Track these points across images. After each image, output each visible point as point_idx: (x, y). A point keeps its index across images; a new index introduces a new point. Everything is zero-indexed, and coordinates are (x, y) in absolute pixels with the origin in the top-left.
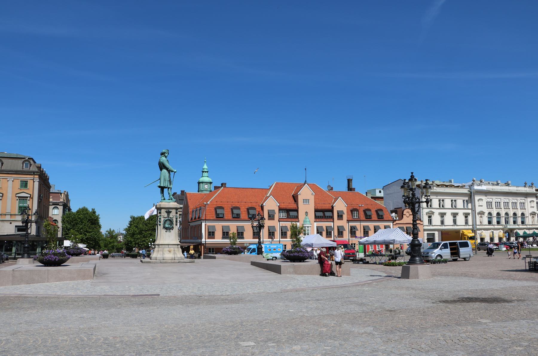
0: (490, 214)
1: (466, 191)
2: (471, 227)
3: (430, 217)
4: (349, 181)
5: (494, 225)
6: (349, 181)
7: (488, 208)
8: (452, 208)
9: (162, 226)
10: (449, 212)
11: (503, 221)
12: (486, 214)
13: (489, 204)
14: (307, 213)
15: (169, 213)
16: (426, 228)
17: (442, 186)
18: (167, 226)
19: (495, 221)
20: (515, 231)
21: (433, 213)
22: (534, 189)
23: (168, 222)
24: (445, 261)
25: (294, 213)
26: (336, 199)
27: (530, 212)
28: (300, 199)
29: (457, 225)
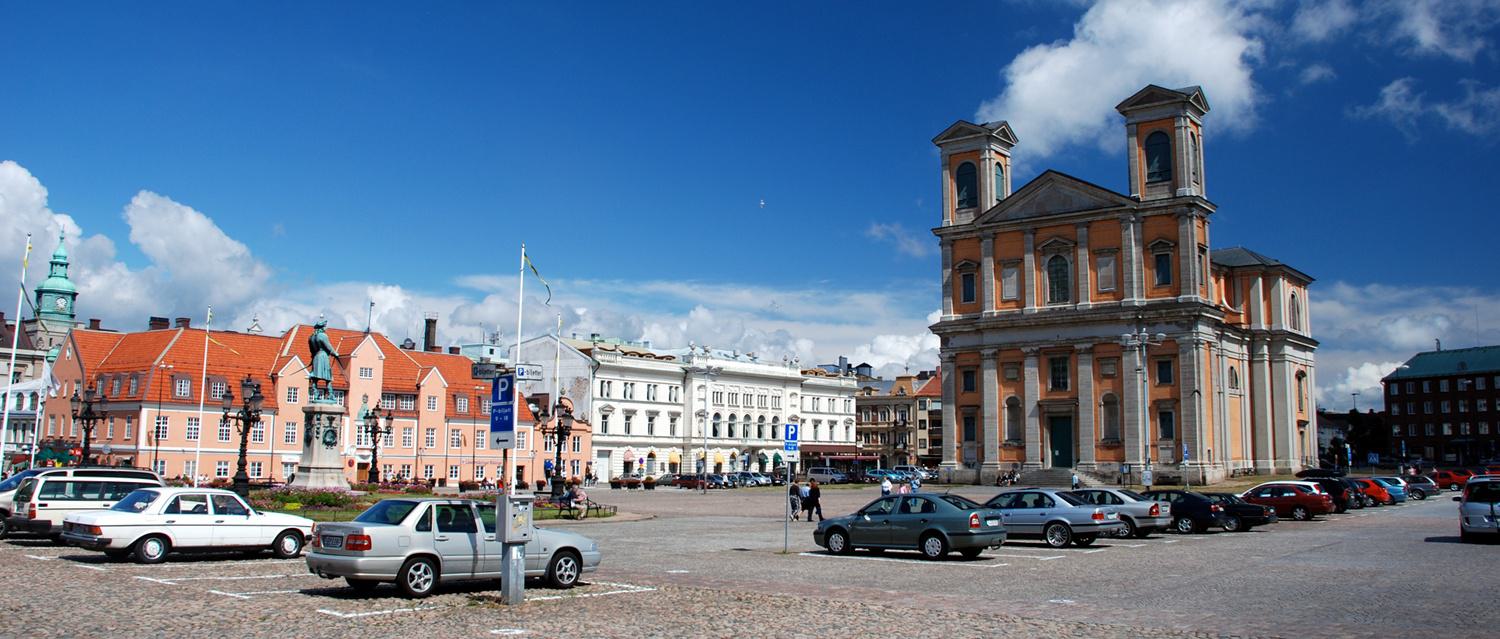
0: (717, 416)
1: (675, 368)
2: (680, 441)
3: (605, 417)
4: (430, 324)
5: (738, 439)
6: (430, 324)
7: (714, 405)
9: (321, 440)
10: (642, 411)
11: (739, 431)
12: (711, 416)
13: (717, 395)
14: (366, 396)
15: (331, 420)
16: (597, 439)
17: (633, 354)
18: (328, 440)
19: (724, 430)
20: (760, 452)
21: (612, 409)
22: (799, 371)
23: (330, 434)
27: (789, 415)
28: (355, 365)
29: (632, 436)
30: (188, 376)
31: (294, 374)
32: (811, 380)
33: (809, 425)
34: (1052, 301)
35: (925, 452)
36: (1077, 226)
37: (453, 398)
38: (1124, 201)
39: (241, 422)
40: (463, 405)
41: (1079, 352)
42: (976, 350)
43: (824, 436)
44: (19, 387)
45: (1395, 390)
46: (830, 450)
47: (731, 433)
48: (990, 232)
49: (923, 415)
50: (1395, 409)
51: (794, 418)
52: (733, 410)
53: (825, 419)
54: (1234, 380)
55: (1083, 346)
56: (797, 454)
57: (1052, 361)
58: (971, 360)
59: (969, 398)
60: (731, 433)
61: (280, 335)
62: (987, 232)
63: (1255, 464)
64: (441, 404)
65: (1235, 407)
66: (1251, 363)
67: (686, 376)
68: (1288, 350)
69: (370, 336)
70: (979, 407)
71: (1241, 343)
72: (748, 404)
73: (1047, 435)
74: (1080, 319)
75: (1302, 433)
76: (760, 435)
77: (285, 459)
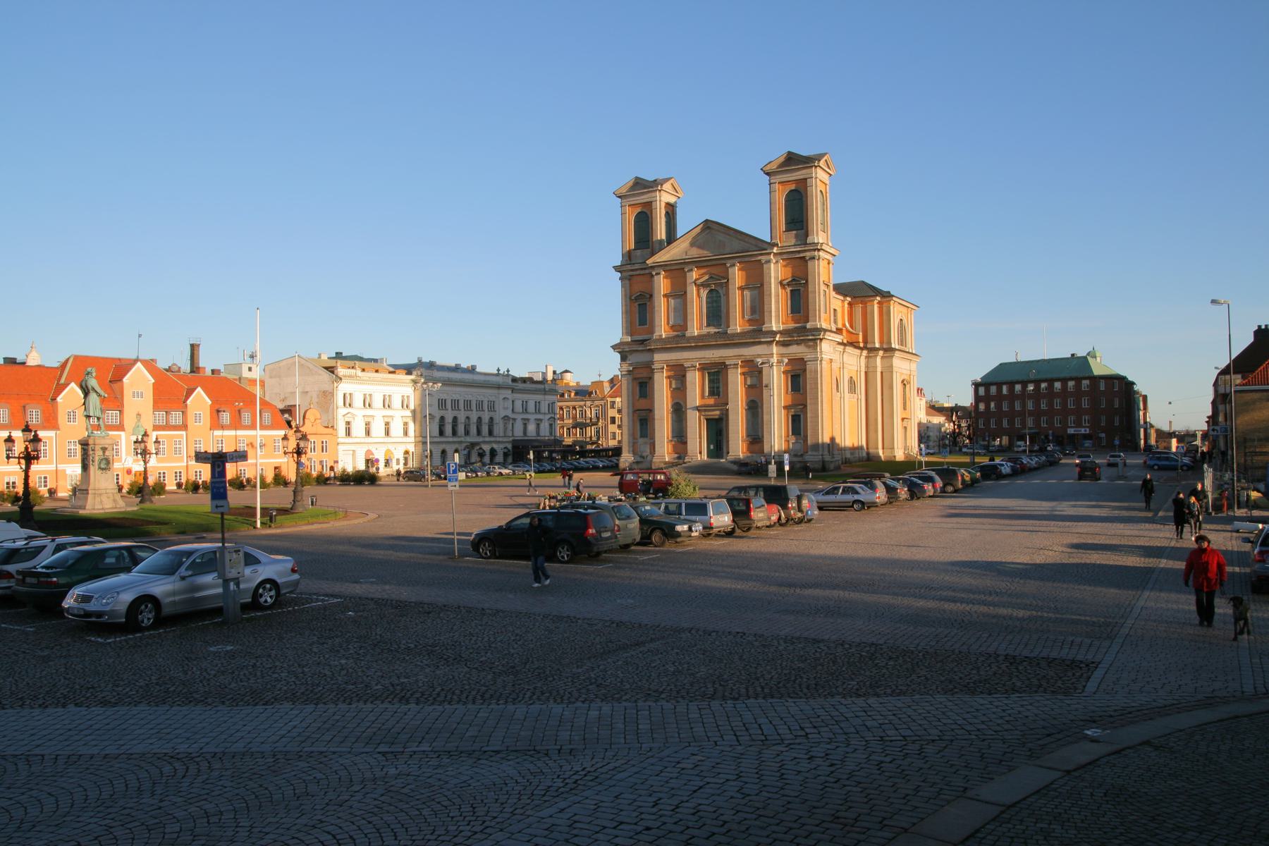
4: (194, 348)
6: (194, 348)
11: (461, 429)
21: (354, 416)
24: (1002, 476)
26: (190, 392)
32: (521, 386)
34: (708, 325)
39: (23, 461)
45: (982, 391)
50: (982, 407)
51: (506, 418)
52: (456, 413)
56: (510, 446)
59: (642, 404)
61: (56, 365)
69: (139, 364)
70: (650, 411)
76: (479, 433)
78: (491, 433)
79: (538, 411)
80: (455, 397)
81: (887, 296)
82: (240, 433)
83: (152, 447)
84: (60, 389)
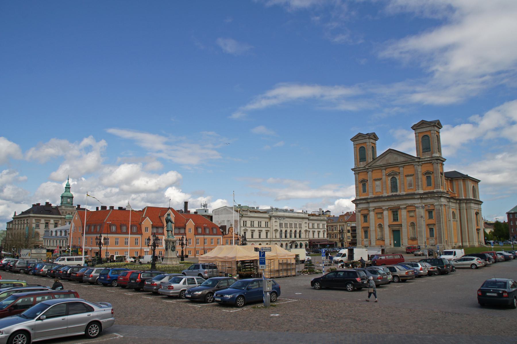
2: (269, 240)
8: (259, 227)
11: (288, 235)
12: (279, 231)
13: (281, 225)
21: (247, 230)
25: (240, 242)
26: (187, 221)
30: (125, 225)
31: (147, 223)
32: (312, 218)
33: (311, 233)
35: (350, 240)
36: (399, 167)
37: (196, 228)
38: (415, 159)
40: (200, 230)
41: (401, 209)
42: (367, 209)
43: (316, 236)
44: (57, 228)
46: (319, 241)
47: (286, 237)
48: (371, 170)
49: (349, 228)
51: (306, 231)
53: (316, 230)
54: (454, 217)
55: (379, 233)
56: (308, 242)
57: (393, 211)
58: (366, 212)
60: (286, 237)
62: (370, 170)
63: (462, 244)
64: (193, 231)
65: (454, 225)
66: (460, 210)
67: (270, 218)
68: (472, 205)
71: (456, 203)
72: (296, 227)
73: (392, 236)
74: (401, 198)
75: (478, 233)
76: (295, 237)
77: (145, 250)
78: (300, 237)
79: (318, 228)
80: (291, 222)
81: (476, 181)
82: (205, 237)
83: (185, 242)
84: (143, 219)
